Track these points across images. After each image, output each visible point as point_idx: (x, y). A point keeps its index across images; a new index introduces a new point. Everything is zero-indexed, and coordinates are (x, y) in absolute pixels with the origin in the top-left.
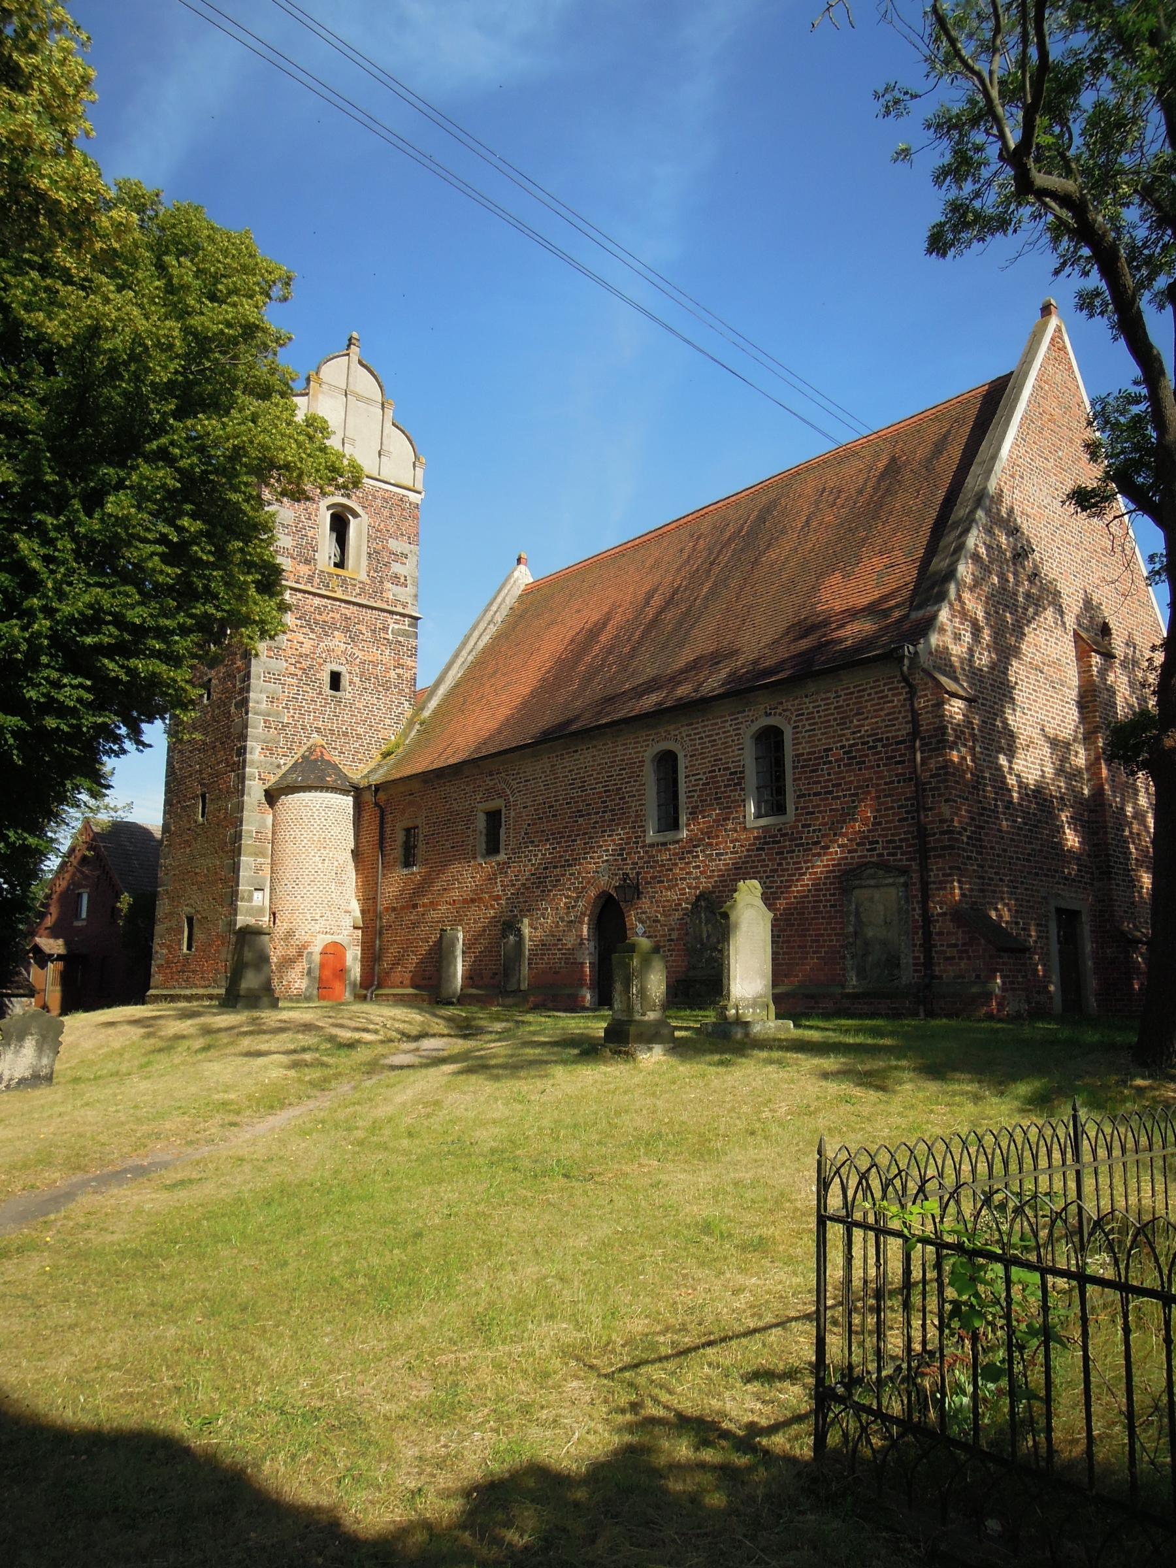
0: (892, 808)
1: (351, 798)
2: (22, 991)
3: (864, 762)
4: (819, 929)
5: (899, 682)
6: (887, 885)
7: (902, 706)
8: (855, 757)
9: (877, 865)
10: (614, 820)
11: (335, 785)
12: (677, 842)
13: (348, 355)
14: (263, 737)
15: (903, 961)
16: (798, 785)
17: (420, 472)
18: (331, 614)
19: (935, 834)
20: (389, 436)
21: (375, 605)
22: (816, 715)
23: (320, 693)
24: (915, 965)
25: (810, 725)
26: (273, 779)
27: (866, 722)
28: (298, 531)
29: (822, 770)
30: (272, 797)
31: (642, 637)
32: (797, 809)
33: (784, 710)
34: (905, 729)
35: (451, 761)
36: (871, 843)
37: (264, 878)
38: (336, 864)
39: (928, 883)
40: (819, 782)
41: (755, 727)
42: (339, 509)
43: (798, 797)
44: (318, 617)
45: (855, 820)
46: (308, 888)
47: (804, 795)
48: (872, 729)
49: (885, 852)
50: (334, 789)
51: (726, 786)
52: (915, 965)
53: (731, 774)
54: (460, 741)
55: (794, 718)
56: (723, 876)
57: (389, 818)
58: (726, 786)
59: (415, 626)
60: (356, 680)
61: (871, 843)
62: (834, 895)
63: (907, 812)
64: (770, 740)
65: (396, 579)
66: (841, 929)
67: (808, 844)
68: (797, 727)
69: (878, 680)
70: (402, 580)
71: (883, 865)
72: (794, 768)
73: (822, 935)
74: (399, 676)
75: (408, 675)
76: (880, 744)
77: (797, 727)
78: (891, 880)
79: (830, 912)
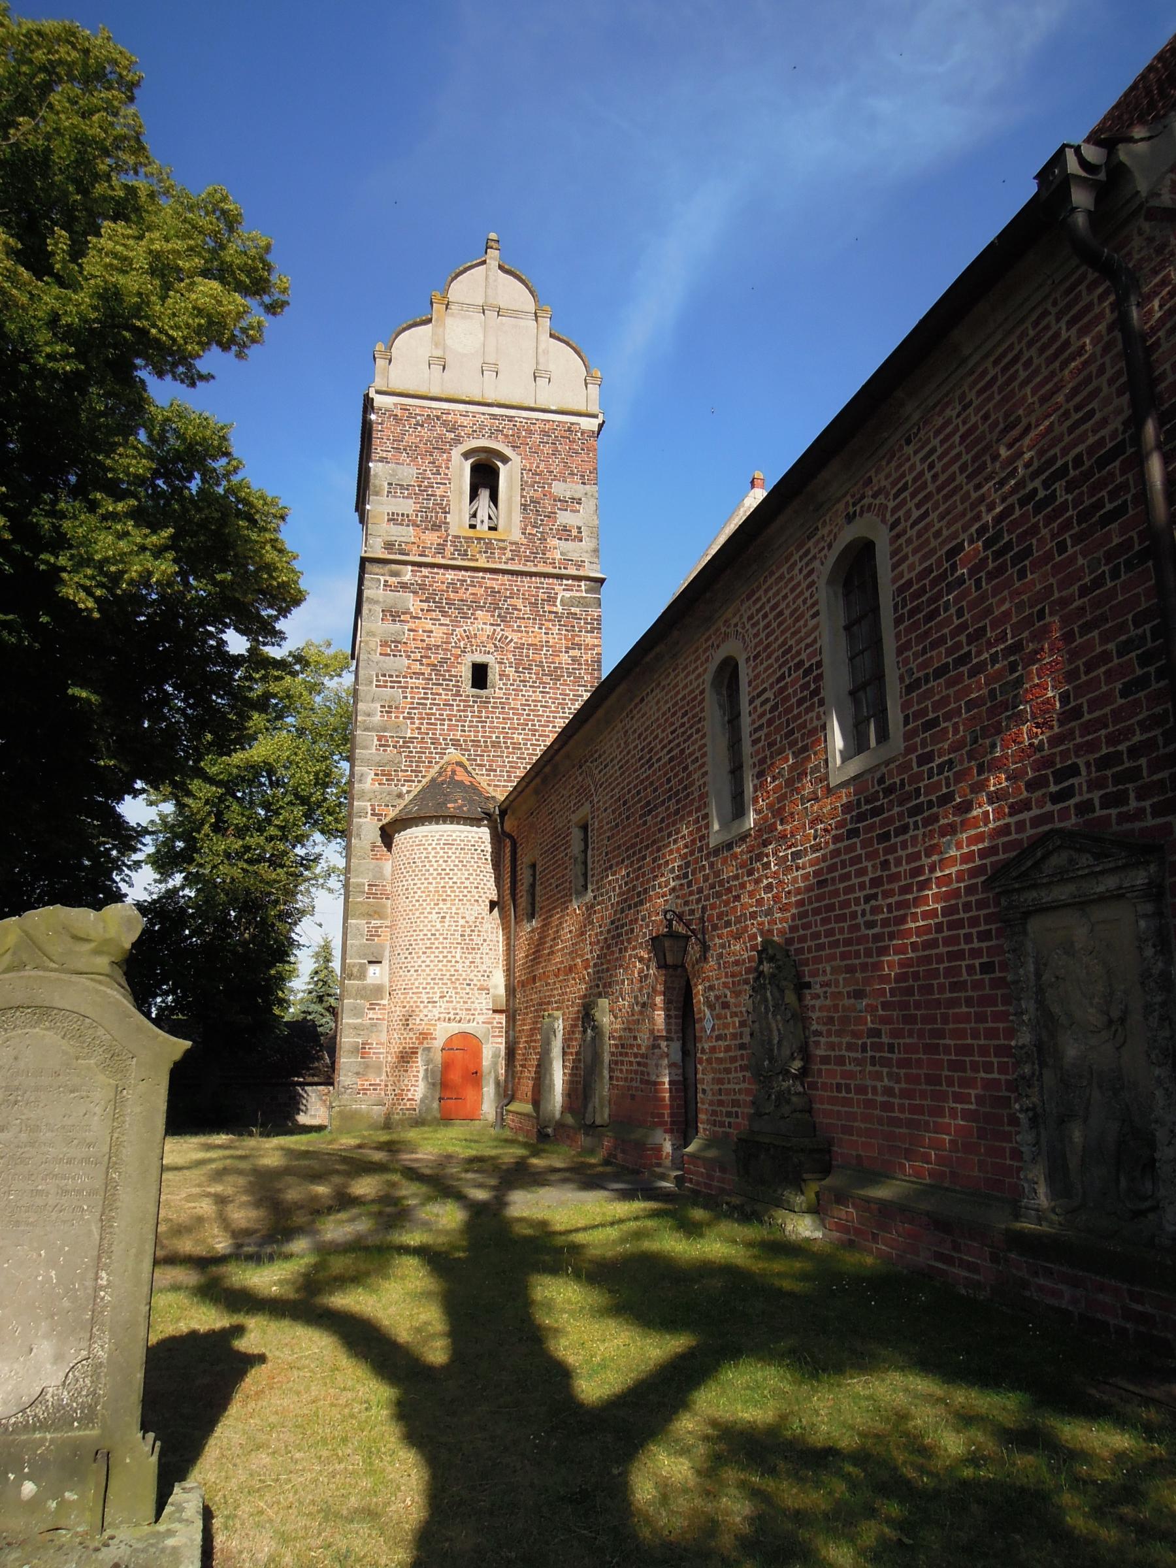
1: (487, 830)
2: (316, 1079)
6: (1102, 899)
8: (1009, 546)
9: (1068, 838)
11: (458, 813)
12: (743, 838)
14: (377, 759)
17: (594, 390)
20: (546, 352)
21: (534, 569)
23: (458, 694)
26: (392, 814)
28: (422, 490)
30: (387, 835)
33: (875, 496)
37: (382, 947)
38: (462, 922)
42: (483, 456)
44: (452, 595)
45: (1019, 718)
46: (423, 958)
48: (1041, 453)
49: (1096, 796)
50: (454, 819)
55: (891, 504)
56: (956, 893)
60: (510, 671)
65: (565, 533)
67: (930, 804)
70: (574, 532)
76: (1059, 485)
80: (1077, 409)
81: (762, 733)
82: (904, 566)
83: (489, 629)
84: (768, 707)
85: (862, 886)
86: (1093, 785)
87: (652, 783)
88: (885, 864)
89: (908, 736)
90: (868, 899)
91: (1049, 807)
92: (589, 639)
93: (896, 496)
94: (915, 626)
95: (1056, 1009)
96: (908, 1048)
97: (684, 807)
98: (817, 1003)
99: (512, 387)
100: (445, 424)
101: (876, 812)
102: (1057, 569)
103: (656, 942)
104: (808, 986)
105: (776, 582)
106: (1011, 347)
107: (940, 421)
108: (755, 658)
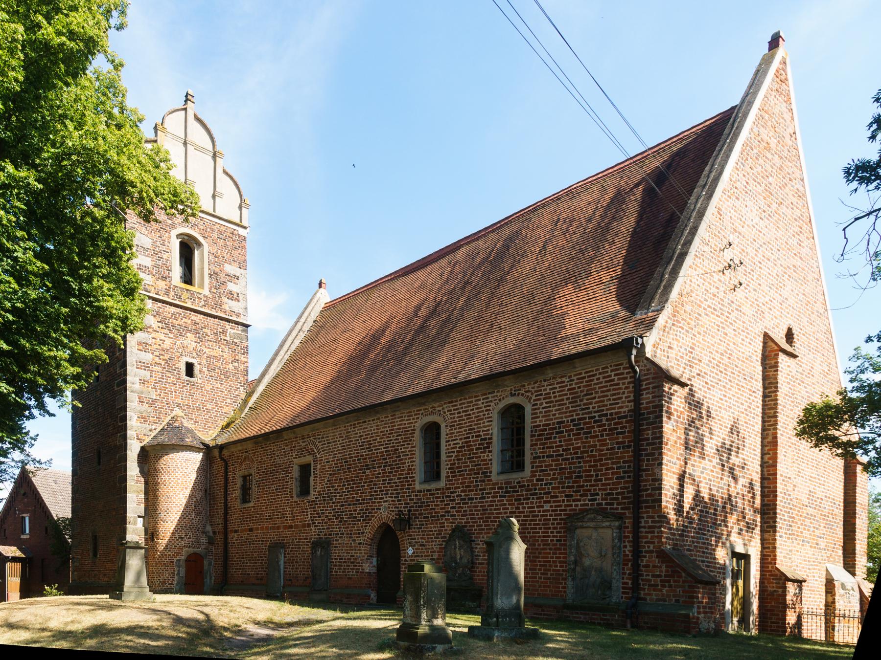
0: (612, 468)
1: (201, 454)
3: (590, 433)
4: (547, 557)
5: (625, 368)
7: (626, 388)
8: (583, 428)
9: (596, 512)
10: (392, 472)
11: (192, 444)
13: (185, 109)
15: (614, 584)
16: (535, 449)
18: (184, 320)
19: (648, 490)
22: (553, 395)
24: (623, 588)
26: (147, 440)
27: (594, 401)
28: (156, 254)
29: (555, 438)
31: (413, 339)
32: (533, 467)
33: (526, 392)
34: (627, 407)
35: (274, 428)
36: (592, 495)
39: (639, 527)
40: (552, 447)
41: (502, 405)
43: (534, 458)
44: (174, 321)
47: (539, 457)
49: (604, 502)
51: (477, 449)
52: (623, 588)
53: (482, 440)
54: (281, 415)
55: (534, 398)
57: (231, 468)
58: (477, 449)
59: (247, 332)
60: (205, 369)
61: (592, 495)
62: (560, 532)
63: (624, 472)
64: (513, 417)
65: (231, 296)
66: (564, 558)
68: (536, 404)
69: (607, 367)
70: (235, 296)
71: (601, 512)
72: (532, 436)
73: (549, 562)
76: (604, 418)
77: (536, 404)
78: (608, 524)
79: (556, 545)
80: (614, 400)
88: (518, 508)
91: (587, 502)
92: (242, 358)
103: (520, 533)
107: (559, 380)
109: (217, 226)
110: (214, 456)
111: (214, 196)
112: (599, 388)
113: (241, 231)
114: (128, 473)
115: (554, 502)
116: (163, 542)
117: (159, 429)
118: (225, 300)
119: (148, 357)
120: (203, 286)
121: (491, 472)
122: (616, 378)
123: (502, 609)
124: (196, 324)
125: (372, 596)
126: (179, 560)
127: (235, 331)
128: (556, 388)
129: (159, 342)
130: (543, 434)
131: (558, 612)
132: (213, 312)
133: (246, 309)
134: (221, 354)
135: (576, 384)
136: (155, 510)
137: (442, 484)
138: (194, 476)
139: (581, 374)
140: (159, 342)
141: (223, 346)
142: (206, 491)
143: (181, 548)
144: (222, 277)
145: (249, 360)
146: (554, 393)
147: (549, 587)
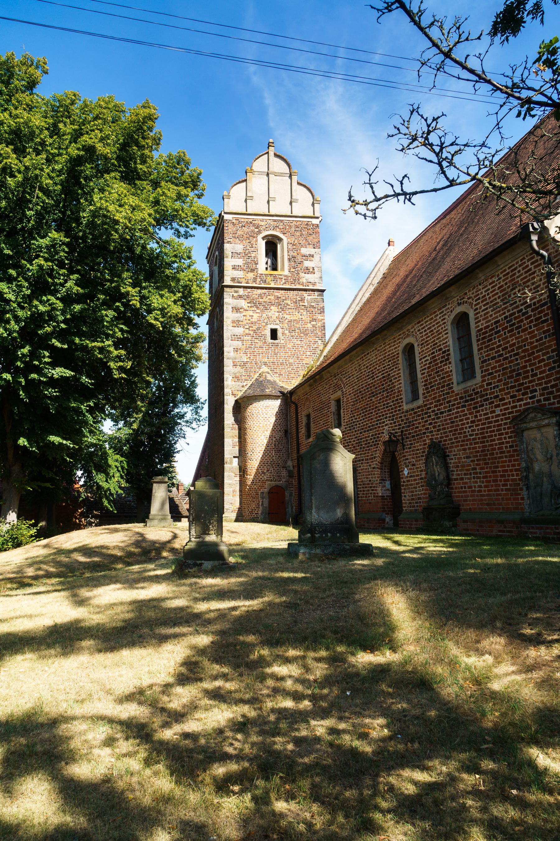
1: (279, 400)
3: (520, 327)
6: (544, 426)
8: (514, 324)
9: (535, 409)
11: (270, 393)
13: (268, 153)
18: (269, 297)
22: (487, 297)
25: (484, 306)
26: (240, 394)
28: (246, 254)
29: (495, 338)
32: (482, 372)
33: (468, 299)
40: (493, 349)
43: (483, 362)
44: (261, 300)
49: (542, 398)
55: (474, 303)
59: (322, 295)
60: (287, 332)
65: (307, 271)
69: (524, 258)
70: (311, 270)
71: (541, 409)
74: (313, 326)
75: (319, 324)
76: (529, 309)
78: (546, 421)
81: (426, 371)
82: (480, 323)
83: (277, 314)
84: (428, 362)
85: (468, 423)
86: (542, 395)
87: (374, 385)
88: (476, 416)
89: (482, 377)
90: (470, 427)
91: (529, 400)
92: (319, 317)
93: (476, 301)
94: (484, 343)
95: (532, 457)
96: (486, 472)
97: (391, 395)
98: (452, 461)
99: (280, 207)
100: (254, 225)
101: (472, 400)
102: (529, 333)
104: (448, 456)
105: (430, 320)
106: (514, 265)
107: (491, 281)
108: (422, 344)
109: (294, 223)
110: (289, 399)
111: (291, 203)
112: (521, 280)
113: (315, 221)
114: (225, 422)
115: (503, 405)
116: (250, 478)
117: (249, 385)
118: (302, 275)
119: (240, 331)
120: (285, 268)
121: (452, 383)
122: (533, 266)
123: (320, 524)
124: (278, 298)
125: (387, 520)
126: (263, 493)
127: (312, 297)
128: (489, 289)
129: (248, 318)
130: (486, 336)
131: (517, 528)
132: (293, 287)
133: (321, 277)
134: (300, 317)
135: (503, 281)
136: (245, 451)
137: (420, 402)
138: (273, 419)
139: (505, 270)
140: (248, 318)
141: (302, 311)
142: (286, 432)
143: (264, 482)
144: (299, 258)
145: (325, 318)
146: (488, 294)
147: (510, 499)
